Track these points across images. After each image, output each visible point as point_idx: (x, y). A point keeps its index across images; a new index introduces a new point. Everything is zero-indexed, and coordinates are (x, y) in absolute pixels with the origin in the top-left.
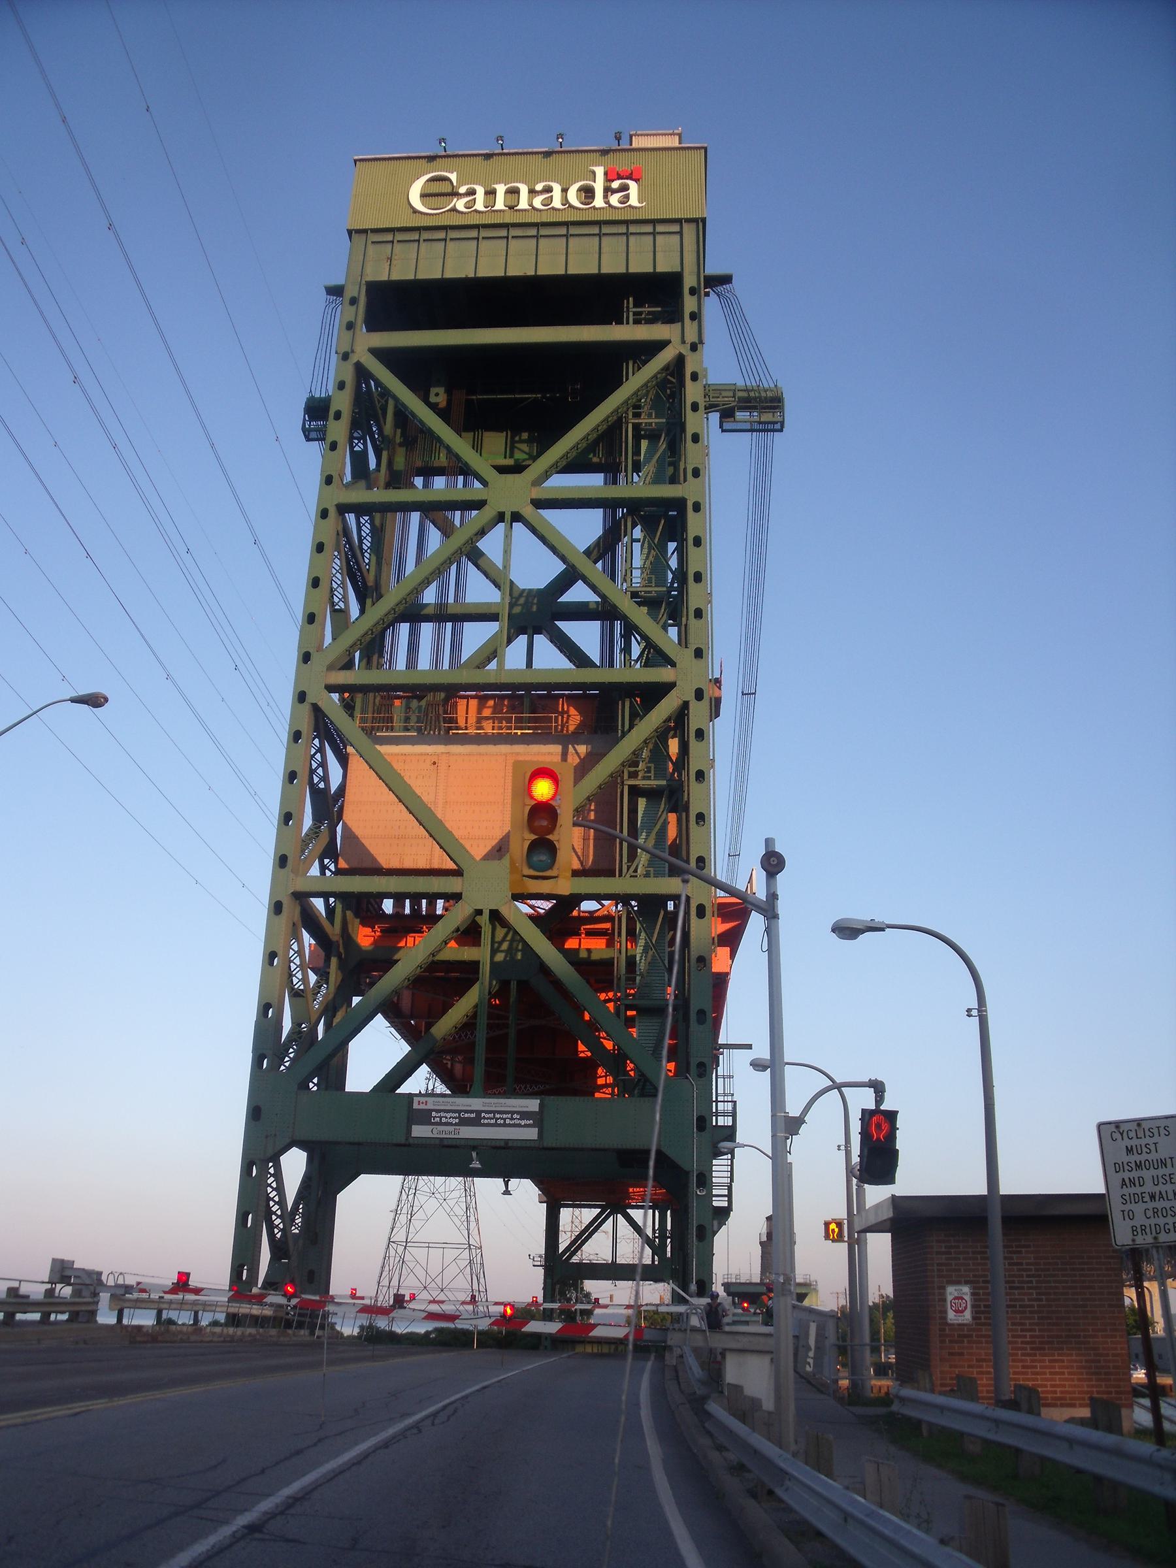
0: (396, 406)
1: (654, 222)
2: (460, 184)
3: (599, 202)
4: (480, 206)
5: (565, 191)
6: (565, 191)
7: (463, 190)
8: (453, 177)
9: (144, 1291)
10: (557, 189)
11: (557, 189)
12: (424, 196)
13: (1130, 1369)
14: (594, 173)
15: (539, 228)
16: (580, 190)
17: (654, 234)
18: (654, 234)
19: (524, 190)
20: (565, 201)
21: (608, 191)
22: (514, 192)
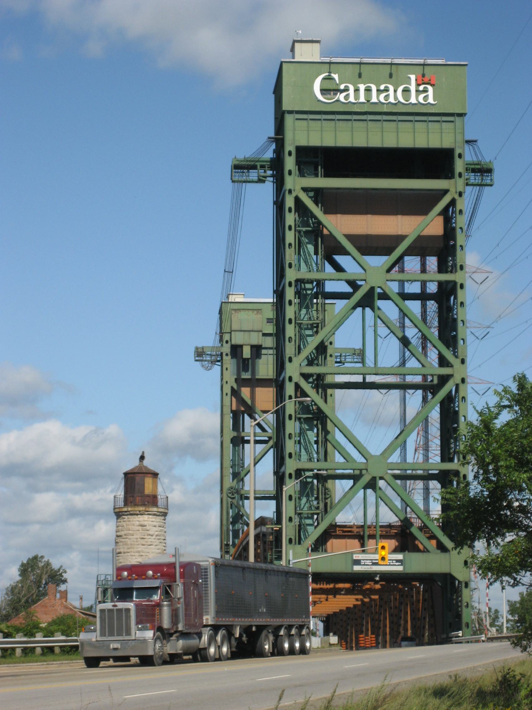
2: (341, 83)
5: (395, 91)
11: (352, 88)
19: (374, 88)
20: (396, 98)
22: (368, 90)
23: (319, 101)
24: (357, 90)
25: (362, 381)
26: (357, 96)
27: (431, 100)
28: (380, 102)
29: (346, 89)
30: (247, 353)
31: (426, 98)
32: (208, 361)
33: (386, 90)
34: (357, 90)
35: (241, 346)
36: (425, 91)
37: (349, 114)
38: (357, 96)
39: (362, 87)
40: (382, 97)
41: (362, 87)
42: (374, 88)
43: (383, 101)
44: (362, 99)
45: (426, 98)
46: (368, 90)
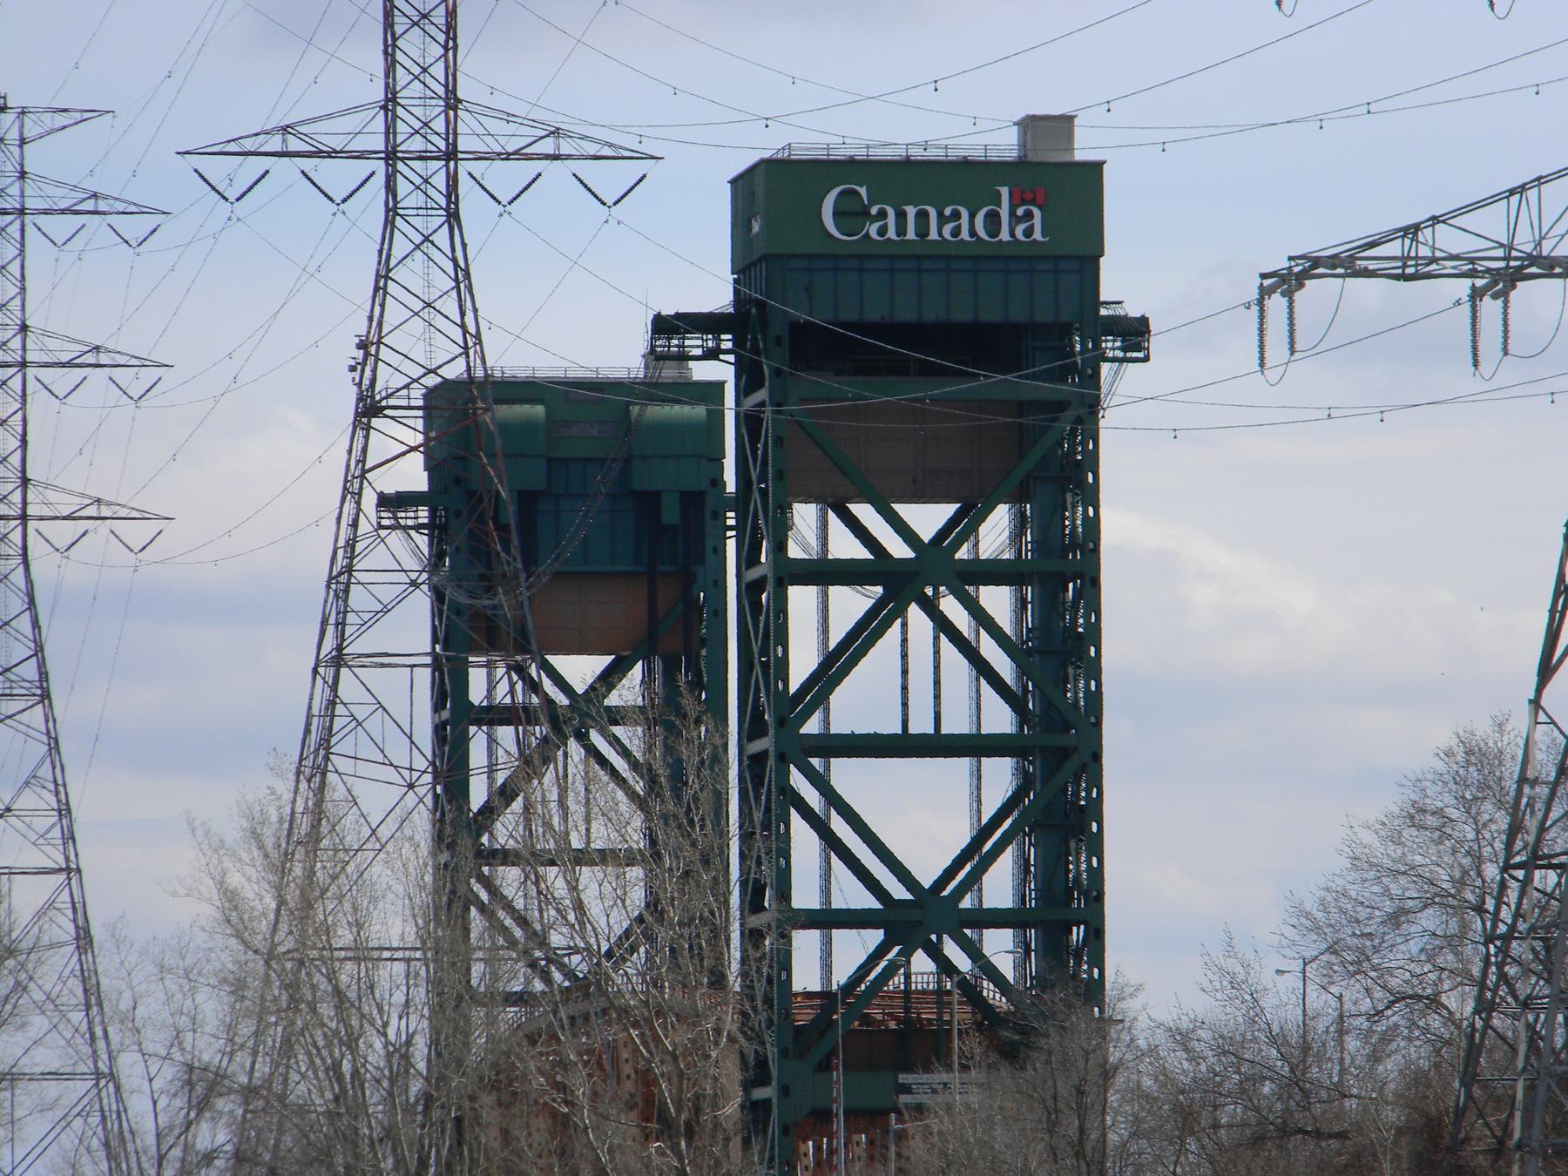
0: (747, 394)
1: (1057, 258)
2: (872, 203)
3: (1005, 235)
4: (891, 234)
5: (972, 216)
6: (972, 216)
7: (874, 210)
8: (863, 191)
9: (520, 1158)
10: (964, 213)
11: (964, 213)
12: (837, 214)
13: (740, 325)
14: (999, 195)
15: (951, 259)
16: (987, 216)
17: (892, 271)
18: (892, 271)
19: (933, 213)
20: (973, 233)
21: (1015, 219)
22: (922, 216)
23: (831, 236)
24: (901, 216)
25: (899, 731)
26: (901, 230)
27: (1037, 235)
28: (945, 240)
29: (882, 214)
30: (670, 513)
31: (1029, 232)
32: (1330, 1136)
33: (956, 215)
34: (901, 216)
35: (657, 495)
36: (1029, 215)
37: (893, 259)
38: (901, 230)
39: (911, 211)
40: (1019, 231)
41: (911, 211)
42: (933, 213)
43: (1022, 238)
44: (911, 235)
45: (1029, 232)
46: (922, 216)
